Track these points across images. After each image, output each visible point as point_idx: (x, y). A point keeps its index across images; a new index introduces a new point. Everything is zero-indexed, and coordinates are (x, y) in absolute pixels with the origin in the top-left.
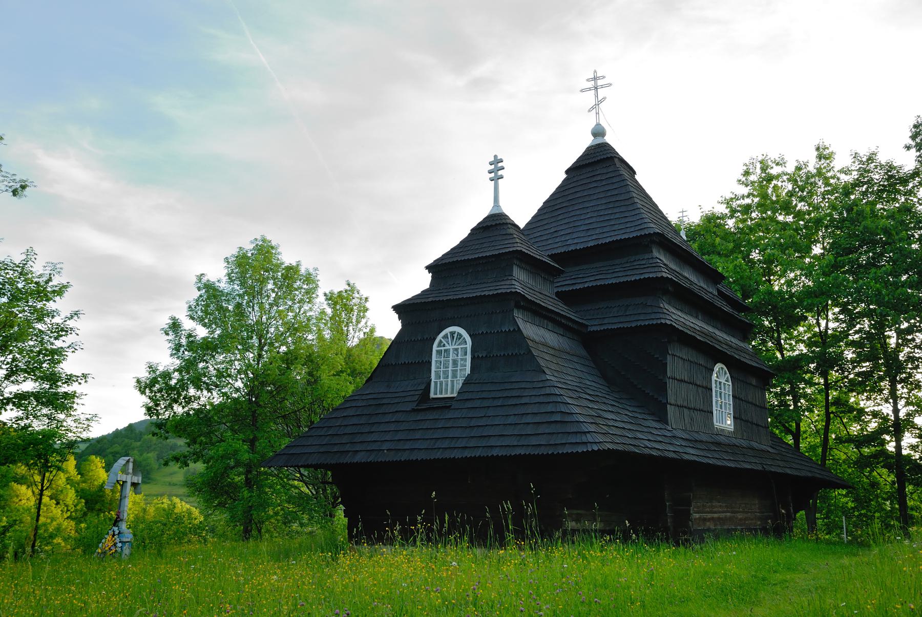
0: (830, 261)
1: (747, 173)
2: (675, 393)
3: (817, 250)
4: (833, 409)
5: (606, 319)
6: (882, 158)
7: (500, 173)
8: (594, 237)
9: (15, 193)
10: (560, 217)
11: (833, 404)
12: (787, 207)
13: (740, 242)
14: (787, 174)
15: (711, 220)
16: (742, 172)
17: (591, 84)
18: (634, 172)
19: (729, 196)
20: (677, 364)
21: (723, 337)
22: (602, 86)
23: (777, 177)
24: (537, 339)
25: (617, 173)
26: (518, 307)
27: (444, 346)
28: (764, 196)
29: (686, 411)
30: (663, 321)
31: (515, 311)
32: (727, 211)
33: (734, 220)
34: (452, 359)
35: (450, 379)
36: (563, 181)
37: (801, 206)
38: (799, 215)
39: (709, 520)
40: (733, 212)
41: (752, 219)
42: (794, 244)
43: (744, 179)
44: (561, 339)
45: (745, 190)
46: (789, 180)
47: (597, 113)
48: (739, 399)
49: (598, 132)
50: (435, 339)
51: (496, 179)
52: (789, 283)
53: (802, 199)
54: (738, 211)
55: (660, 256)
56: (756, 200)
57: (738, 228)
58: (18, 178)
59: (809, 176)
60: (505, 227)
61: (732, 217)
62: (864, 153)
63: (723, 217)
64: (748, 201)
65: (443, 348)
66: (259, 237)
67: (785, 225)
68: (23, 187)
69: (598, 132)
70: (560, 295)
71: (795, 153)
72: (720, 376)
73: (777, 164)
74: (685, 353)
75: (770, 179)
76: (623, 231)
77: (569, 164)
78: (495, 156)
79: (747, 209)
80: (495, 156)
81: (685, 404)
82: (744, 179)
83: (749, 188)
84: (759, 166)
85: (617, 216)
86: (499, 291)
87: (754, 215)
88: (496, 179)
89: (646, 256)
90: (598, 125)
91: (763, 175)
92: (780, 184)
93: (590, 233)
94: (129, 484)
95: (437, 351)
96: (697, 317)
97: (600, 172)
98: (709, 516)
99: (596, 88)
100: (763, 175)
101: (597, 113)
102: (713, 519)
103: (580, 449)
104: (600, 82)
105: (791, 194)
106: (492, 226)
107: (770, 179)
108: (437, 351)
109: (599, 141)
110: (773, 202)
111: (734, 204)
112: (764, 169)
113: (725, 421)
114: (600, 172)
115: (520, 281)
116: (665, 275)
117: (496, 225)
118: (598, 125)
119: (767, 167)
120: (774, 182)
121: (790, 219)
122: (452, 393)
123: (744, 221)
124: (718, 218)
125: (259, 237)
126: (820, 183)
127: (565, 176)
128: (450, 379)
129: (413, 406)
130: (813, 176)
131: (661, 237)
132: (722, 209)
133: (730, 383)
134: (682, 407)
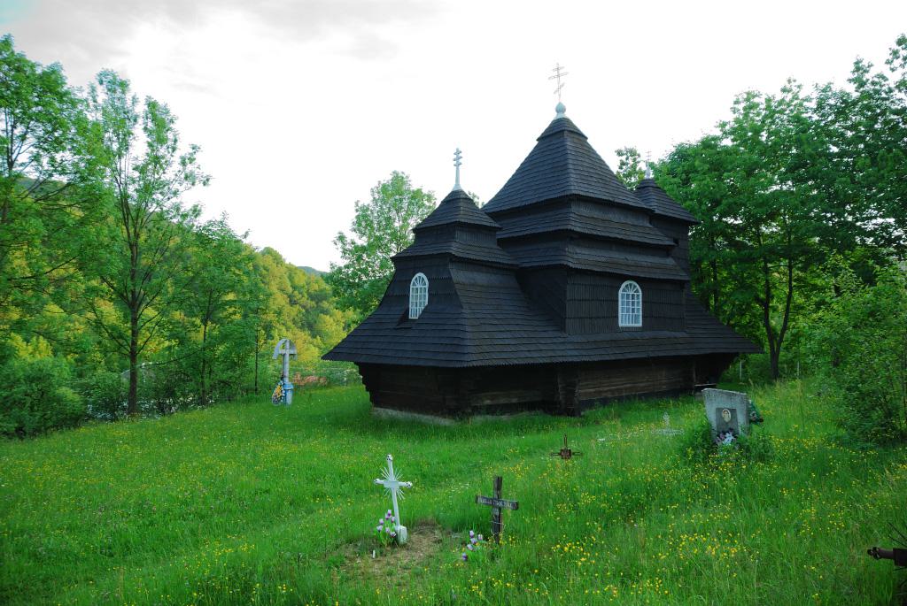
4: (794, 283)
5: (532, 258)
6: (836, 88)
9: (204, 184)
11: (795, 281)
15: (708, 144)
17: (556, 73)
22: (563, 75)
26: (451, 261)
34: (419, 290)
39: (606, 392)
47: (560, 95)
49: (560, 109)
51: (458, 165)
58: (205, 175)
62: (822, 85)
66: (406, 174)
68: (208, 180)
69: (560, 109)
71: (770, 88)
77: (539, 135)
78: (457, 150)
80: (457, 150)
88: (458, 165)
90: (560, 103)
94: (287, 356)
97: (560, 141)
98: (606, 389)
99: (558, 76)
101: (560, 95)
102: (610, 390)
103: (458, 365)
104: (561, 72)
109: (560, 116)
114: (560, 141)
118: (560, 103)
125: (406, 174)
127: (537, 142)
129: (394, 326)
132: (718, 133)
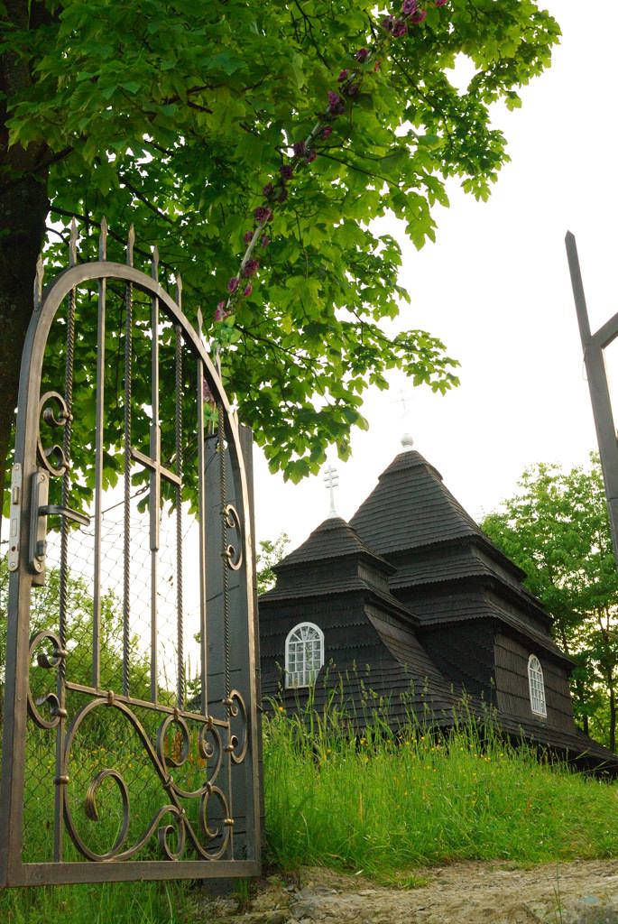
0: (612, 560)
1: (525, 475)
2: (502, 681)
3: (595, 550)
5: (435, 614)
7: (334, 481)
8: (416, 539)
10: (379, 521)
12: (566, 509)
13: (526, 539)
14: (563, 477)
15: (495, 520)
16: (522, 475)
18: (441, 478)
19: (509, 499)
20: (503, 652)
21: (533, 630)
23: (555, 480)
24: (384, 632)
25: (429, 480)
27: (296, 640)
28: (546, 498)
29: (510, 697)
30: (490, 615)
31: (366, 607)
32: (508, 512)
33: (515, 521)
35: (304, 671)
36: (377, 487)
37: (580, 508)
38: (577, 515)
40: (515, 511)
41: (533, 520)
42: (571, 548)
43: (523, 481)
44: (402, 633)
45: (527, 491)
46: (565, 483)
48: (549, 688)
50: (287, 634)
52: (574, 582)
53: (579, 501)
54: (520, 512)
55: (475, 553)
56: (535, 501)
57: (520, 528)
59: (584, 479)
60: (345, 530)
61: (513, 517)
63: (505, 517)
64: (527, 502)
65: (295, 643)
67: (565, 527)
70: (392, 591)
72: (535, 670)
73: (554, 467)
74: (508, 644)
75: (548, 481)
76: (443, 534)
77: (381, 471)
79: (527, 510)
81: (509, 691)
82: (523, 481)
83: (529, 488)
84: (538, 468)
85: (435, 519)
86: (350, 589)
87: (534, 516)
89: (466, 556)
91: (542, 477)
92: (557, 486)
93: (410, 535)
95: (290, 645)
96: (511, 612)
100: (542, 477)
105: (569, 495)
106: (332, 530)
107: (548, 481)
108: (290, 645)
110: (552, 503)
111: (515, 504)
112: (542, 472)
113: (539, 707)
115: (364, 578)
116: (487, 573)
117: (336, 529)
119: (545, 469)
120: (552, 484)
121: (567, 520)
122: (307, 683)
123: (526, 521)
124: (500, 519)
126: (594, 486)
127: (378, 482)
128: (304, 671)
130: (588, 479)
131: (478, 541)
132: (503, 511)
133: (541, 673)
134: (508, 693)
